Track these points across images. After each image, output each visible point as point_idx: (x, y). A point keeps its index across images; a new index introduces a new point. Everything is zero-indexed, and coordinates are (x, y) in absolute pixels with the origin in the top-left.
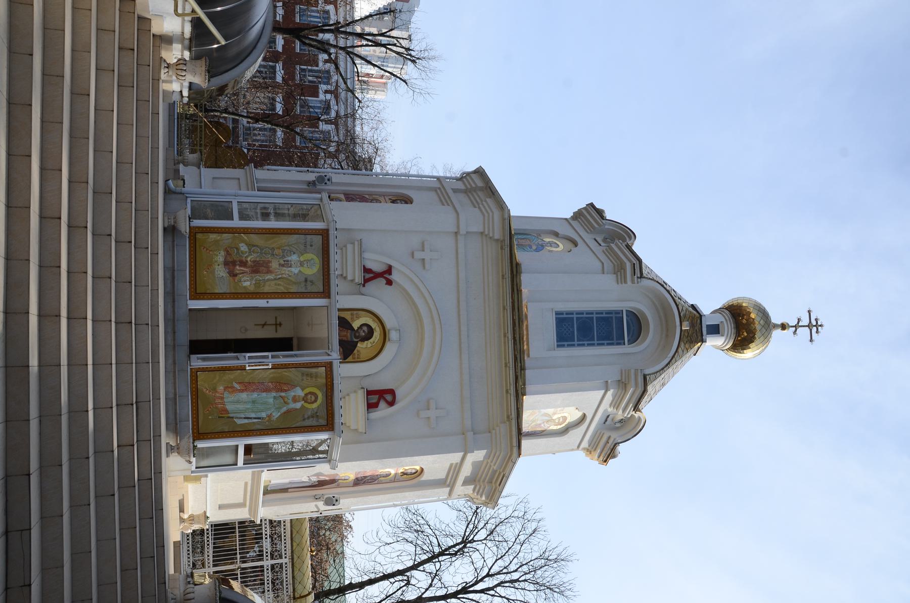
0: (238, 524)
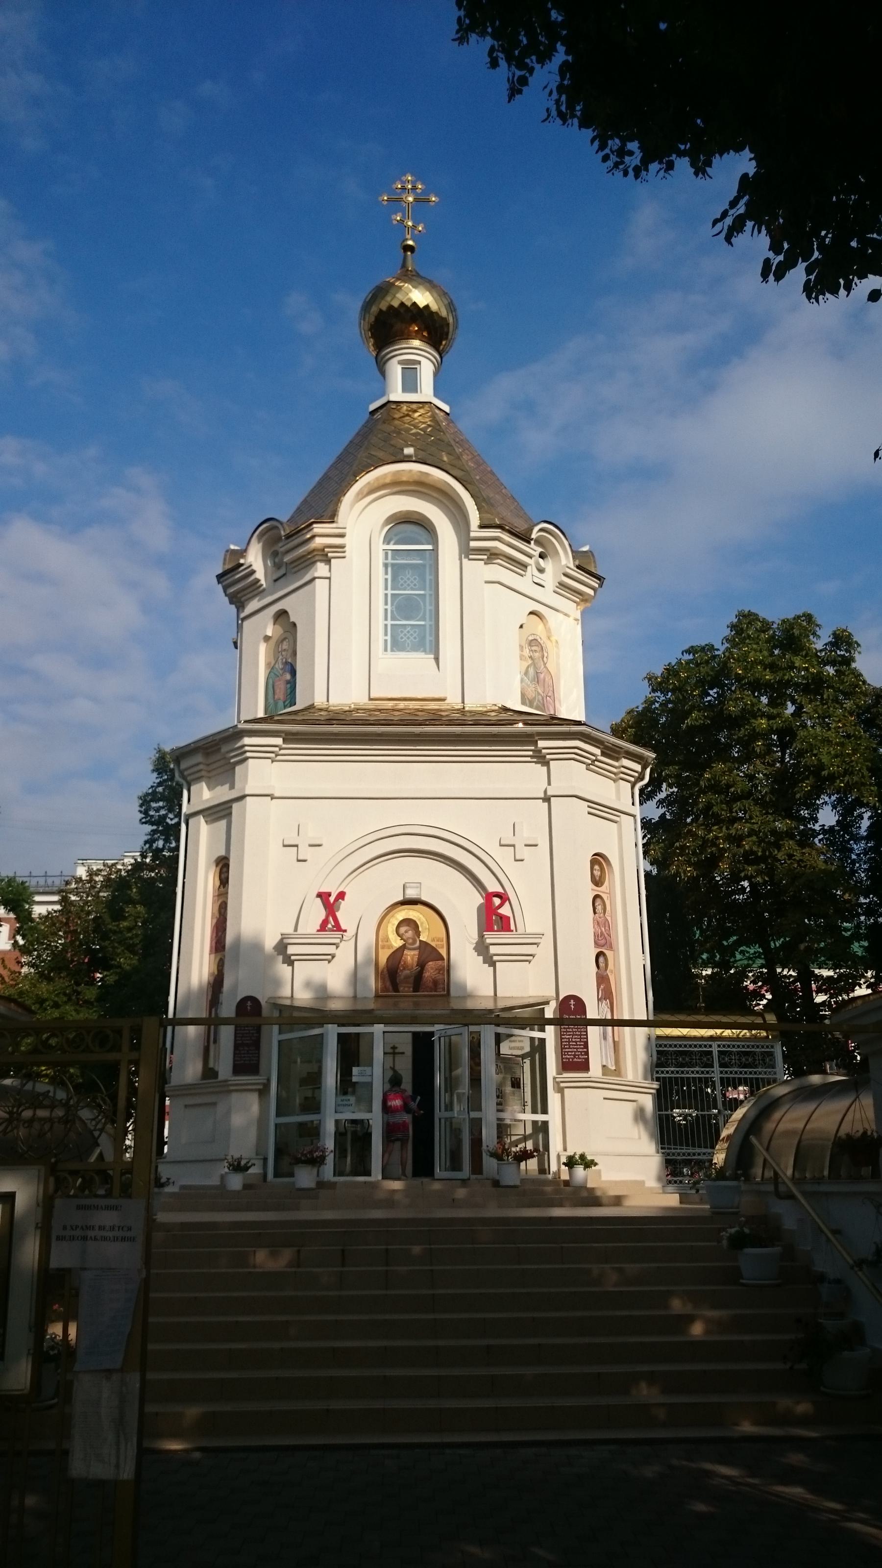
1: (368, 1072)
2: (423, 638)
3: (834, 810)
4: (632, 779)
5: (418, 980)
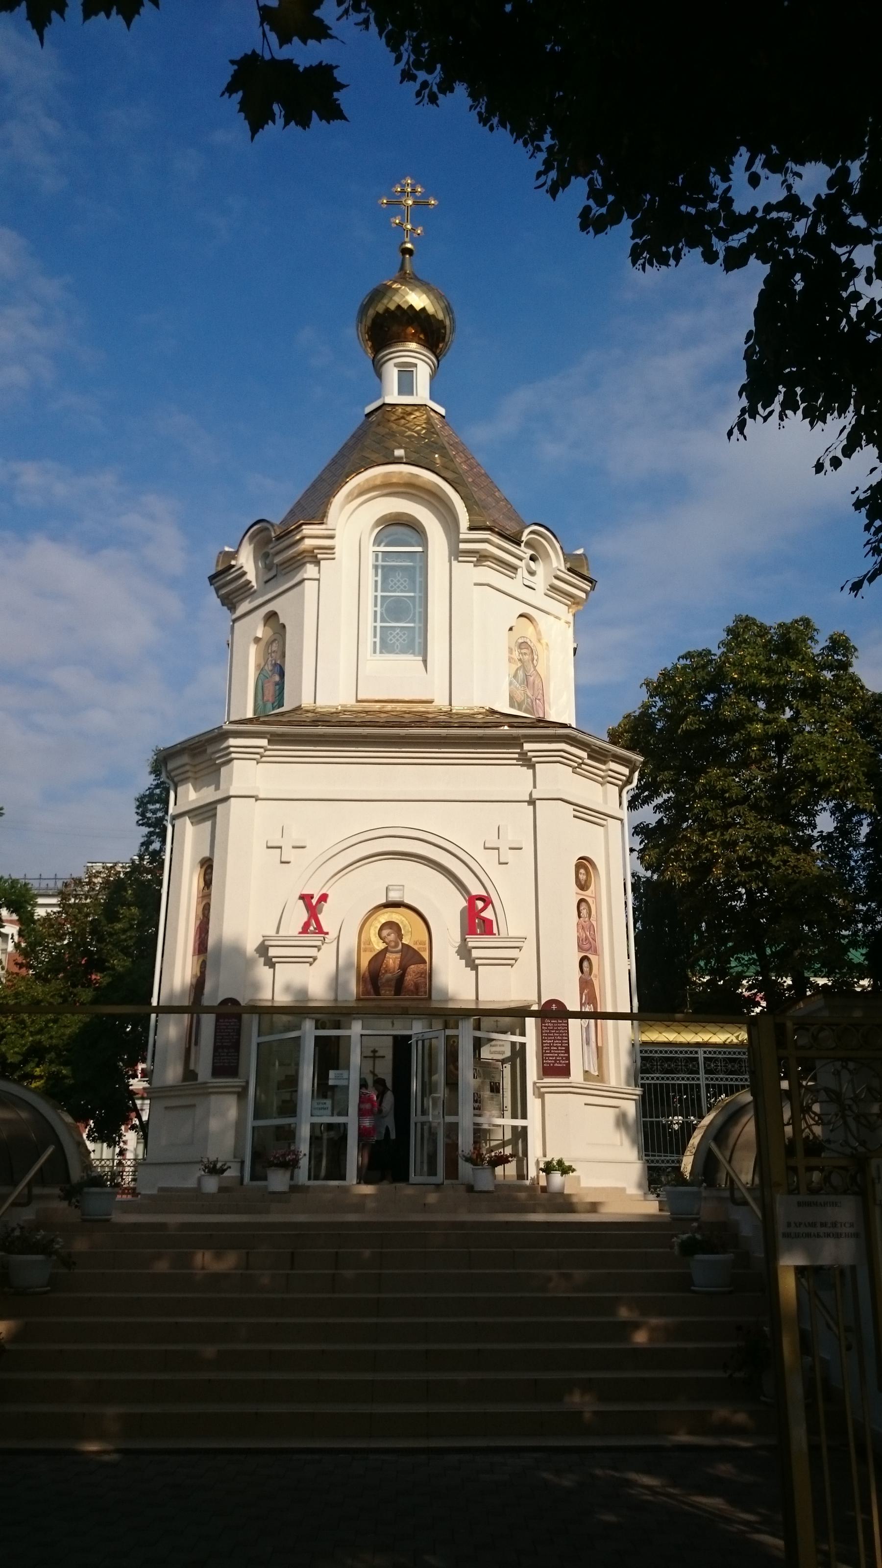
0: (646, 1117)
1: (345, 1076)
2: (413, 640)
3: (833, 817)
4: (620, 783)
5: (399, 984)
